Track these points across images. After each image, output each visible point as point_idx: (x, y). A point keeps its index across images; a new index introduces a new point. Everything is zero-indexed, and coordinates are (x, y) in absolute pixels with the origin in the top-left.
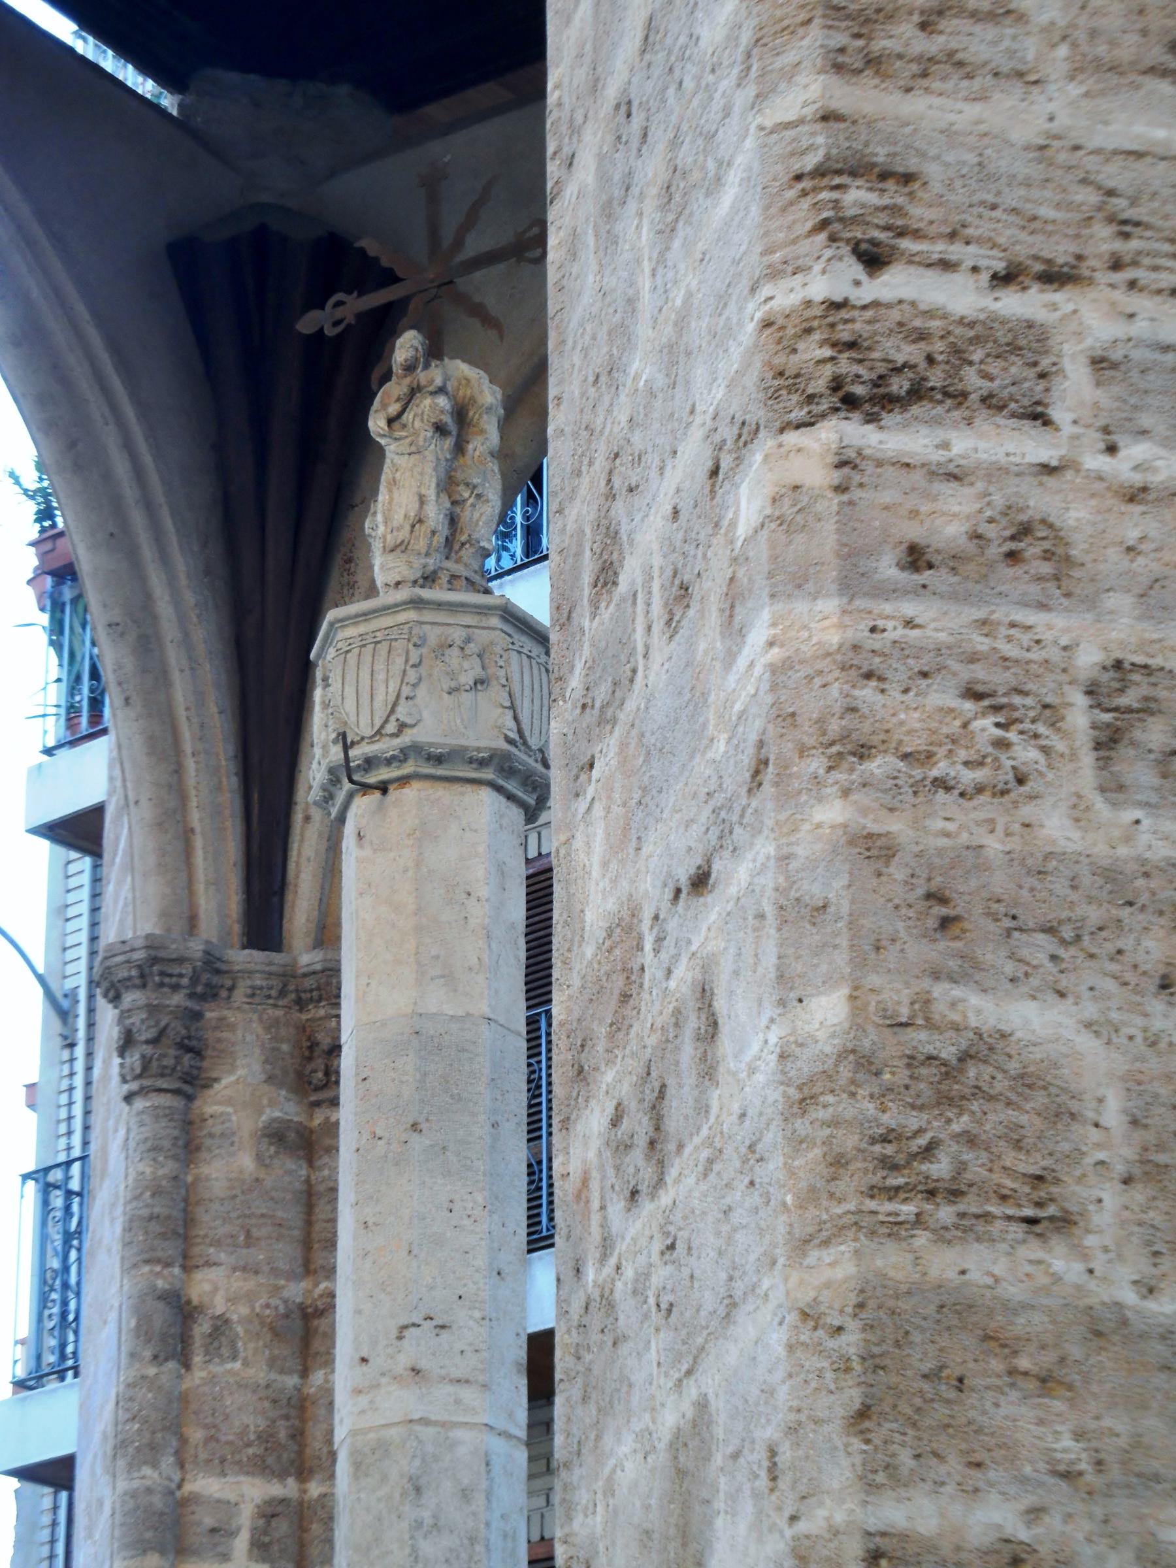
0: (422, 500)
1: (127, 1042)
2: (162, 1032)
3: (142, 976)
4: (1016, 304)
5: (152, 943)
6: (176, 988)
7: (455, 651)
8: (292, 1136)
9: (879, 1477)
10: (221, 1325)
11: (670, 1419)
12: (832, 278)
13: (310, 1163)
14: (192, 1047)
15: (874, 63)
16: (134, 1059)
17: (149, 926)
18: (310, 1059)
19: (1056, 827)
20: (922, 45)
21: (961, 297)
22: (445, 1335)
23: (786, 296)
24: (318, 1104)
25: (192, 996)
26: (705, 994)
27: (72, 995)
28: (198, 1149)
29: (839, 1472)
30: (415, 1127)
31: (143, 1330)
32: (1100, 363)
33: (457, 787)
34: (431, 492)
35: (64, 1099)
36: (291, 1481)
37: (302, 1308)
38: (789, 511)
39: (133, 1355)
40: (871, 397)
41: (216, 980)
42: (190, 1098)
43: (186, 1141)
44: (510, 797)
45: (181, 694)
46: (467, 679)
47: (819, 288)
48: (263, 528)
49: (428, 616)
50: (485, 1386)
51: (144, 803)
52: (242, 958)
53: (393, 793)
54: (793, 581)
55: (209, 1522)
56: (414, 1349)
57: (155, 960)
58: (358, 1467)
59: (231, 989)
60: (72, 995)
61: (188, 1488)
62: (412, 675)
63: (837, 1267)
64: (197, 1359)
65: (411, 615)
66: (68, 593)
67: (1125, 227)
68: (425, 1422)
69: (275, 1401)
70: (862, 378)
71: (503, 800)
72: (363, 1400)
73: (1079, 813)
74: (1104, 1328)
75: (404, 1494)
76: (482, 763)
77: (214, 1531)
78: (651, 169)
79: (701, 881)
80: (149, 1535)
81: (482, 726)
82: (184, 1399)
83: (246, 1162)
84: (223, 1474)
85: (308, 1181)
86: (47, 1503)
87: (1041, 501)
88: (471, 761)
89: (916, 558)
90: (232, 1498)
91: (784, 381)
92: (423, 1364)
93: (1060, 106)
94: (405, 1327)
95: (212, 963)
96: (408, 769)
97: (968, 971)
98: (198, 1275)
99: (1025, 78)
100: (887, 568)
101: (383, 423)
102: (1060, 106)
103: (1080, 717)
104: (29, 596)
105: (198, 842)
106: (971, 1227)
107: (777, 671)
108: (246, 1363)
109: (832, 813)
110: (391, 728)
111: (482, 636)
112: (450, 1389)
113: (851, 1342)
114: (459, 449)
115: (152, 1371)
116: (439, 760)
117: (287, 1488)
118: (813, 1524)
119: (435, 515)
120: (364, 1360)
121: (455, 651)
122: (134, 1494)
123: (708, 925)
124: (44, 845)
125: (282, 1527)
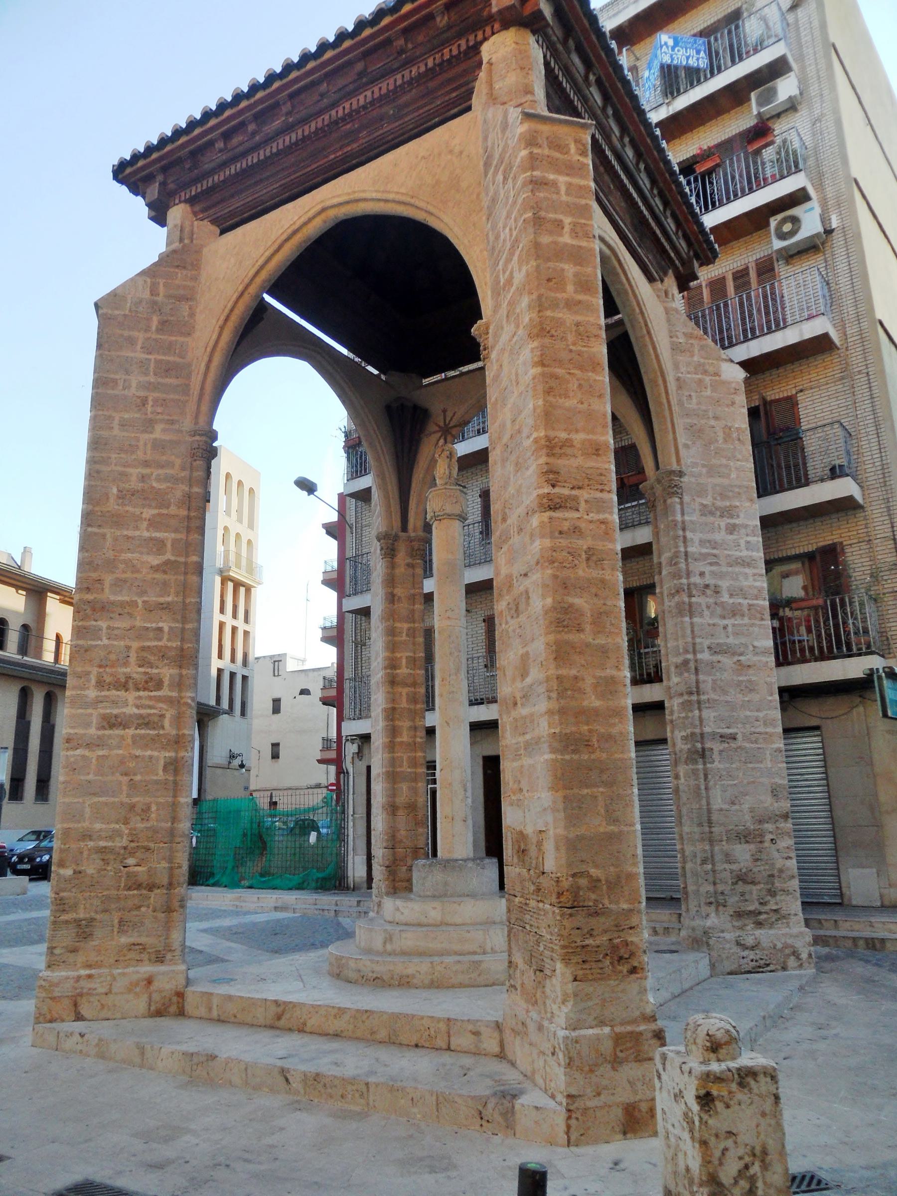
1: (382, 549)
4: (574, 492)
9: (557, 667)
10: (399, 598)
11: (521, 652)
12: (547, 489)
14: (393, 550)
15: (553, 455)
17: (385, 529)
19: (581, 573)
20: (560, 451)
21: (566, 492)
23: (541, 491)
26: (527, 592)
29: (552, 666)
31: (386, 599)
32: (586, 501)
38: (542, 525)
40: (554, 508)
43: (392, 566)
45: (390, 487)
47: (546, 491)
54: (542, 536)
56: (449, 614)
63: (551, 637)
67: (589, 479)
70: (553, 505)
73: (584, 571)
74: (588, 645)
78: (513, 458)
79: (526, 575)
81: (457, 510)
83: (403, 570)
87: (578, 524)
89: (561, 533)
91: (541, 505)
93: (579, 461)
97: (568, 594)
99: (575, 456)
100: (557, 534)
102: (579, 461)
103: (584, 556)
106: (569, 632)
107: (541, 549)
109: (549, 572)
113: (554, 648)
118: (549, 673)
119: (447, 472)
123: (527, 582)
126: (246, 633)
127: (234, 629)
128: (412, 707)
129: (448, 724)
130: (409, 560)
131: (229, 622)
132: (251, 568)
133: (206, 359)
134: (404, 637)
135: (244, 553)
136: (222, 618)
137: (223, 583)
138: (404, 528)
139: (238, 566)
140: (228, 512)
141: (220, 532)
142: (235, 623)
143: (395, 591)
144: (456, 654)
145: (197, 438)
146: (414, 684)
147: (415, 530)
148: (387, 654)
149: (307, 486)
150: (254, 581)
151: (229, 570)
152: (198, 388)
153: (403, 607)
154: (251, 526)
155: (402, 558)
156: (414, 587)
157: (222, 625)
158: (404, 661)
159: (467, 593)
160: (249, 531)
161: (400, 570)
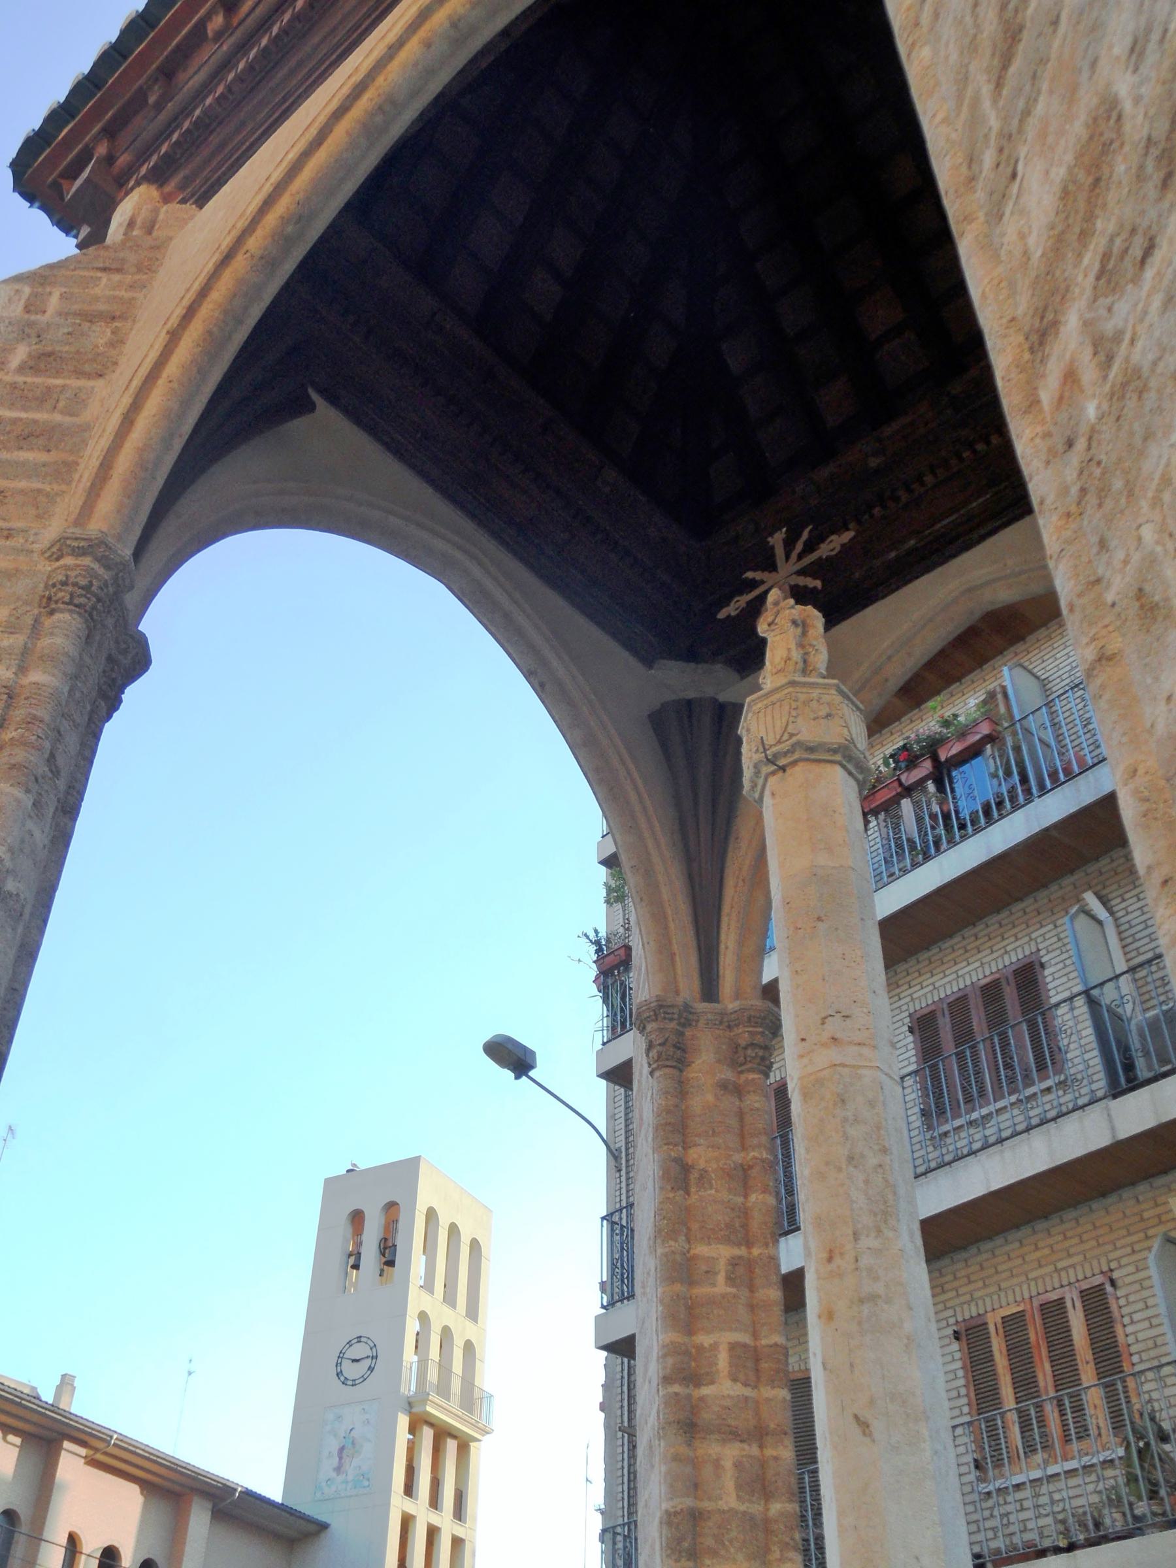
0: (789, 650)
2: (667, 1040)
3: (655, 1015)
5: (659, 999)
6: (671, 1020)
7: (815, 702)
8: (731, 1087)
10: (703, 1174)
13: (741, 1100)
14: (680, 1047)
16: (654, 1053)
18: (736, 1053)
22: (848, 1020)
24: (741, 1072)
25: (679, 1024)
27: (619, 1150)
28: (687, 1093)
30: (819, 919)
31: (666, 1176)
33: (822, 765)
34: (793, 646)
35: (618, 1193)
36: (743, 1248)
37: (741, 1165)
39: (661, 1188)
41: (691, 1017)
42: (681, 1071)
43: (680, 1090)
44: (850, 773)
45: (665, 894)
46: (823, 713)
48: (698, 825)
49: (798, 689)
50: (874, 1047)
51: (652, 943)
52: (701, 1006)
53: (789, 771)
55: (704, 1268)
56: (834, 1026)
57: (661, 1006)
58: (806, 1096)
59: (697, 1021)
60: (619, 1150)
61: (692, 1252)
62: (794, 713)
64: (693, 1190)
65: (791, 689)
66: (610, 982)
68: (843, 1065)
69: (733, 1209)
71: (847, 775)
72: (805, 1060)
75: (835, 1104)
76: (835, 751)
77: (707, 1272)
80: (675, 1274)
82: (688, 1210)
83: (710, 1098)
84: (710, 1244)
85: (740, 1108)
86: (619, 1360)
88: (829, 750)
90: (714, 1255)
92: (838, 1036)
94: (826, 1018)
95: (687, 1007)
96: (796, 756)
98: (691, 1151)
101: (765, 627)
104: (594, 989)
105: (678, 959)
108: (717, 1191)
110: (786, 737)
111: (826, 698)
112: (856, 1048)
114: (804, 633)
115: (671, 1195)
116: (811, 749)
117: (742, 1251)
119: (796, 655)
120: (803, 1040)
121: (815, 702)
122: (666, 1255)
124: (603, 1083)
125: (741, 1270)
126: (457, 1542)
127: (433, 1532)
128: (756, 1508)
129: (863, 1425)
130: (728, 1074)
131: (424, 1516)
132: (471, 1399)
133: (127, 400)
134: (721, 1286)
135: (457, 1367)
136: (409, 1506)
137: (412, 1430)
138: (710, 989)
139: (443, 1389)
140: (428, 1286)
141: (412, 1326)
142: (434, 1519)
143: (693, 1155)
144: (872, 1161)
145: (69, 561)
146: (760, 1434)
147: (737, 996)
148: (673, 1336)
149: (513, 1057)
150: (475, 1426)
151: (425, 1400)
152: (95, 463)
153: (713, 1201)
154: (473, 1313)
155: (706, 1065)
156: (744, 1147)
157: (407, 1522)
158: (723, 1360)
159: (892, 960)
160: (469, 1324)
161: (703, 1098)
